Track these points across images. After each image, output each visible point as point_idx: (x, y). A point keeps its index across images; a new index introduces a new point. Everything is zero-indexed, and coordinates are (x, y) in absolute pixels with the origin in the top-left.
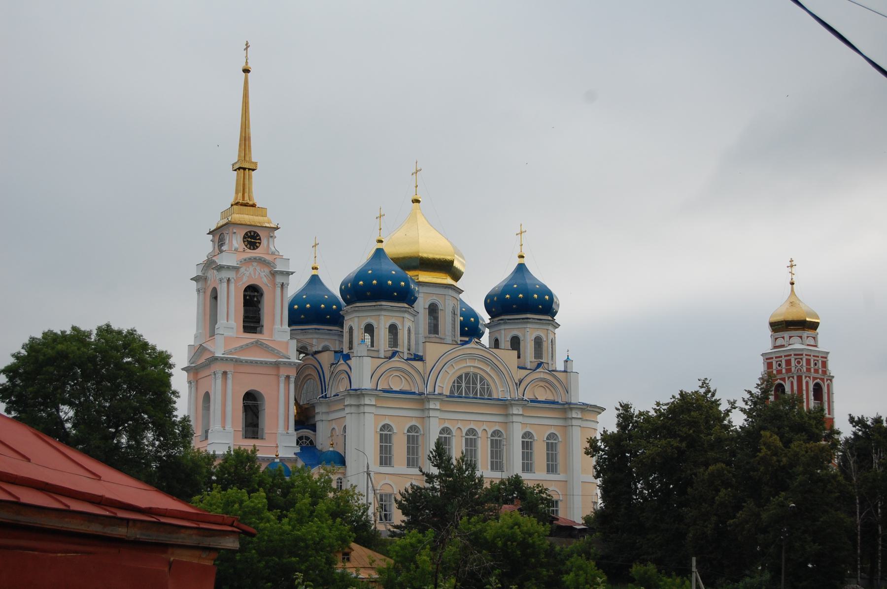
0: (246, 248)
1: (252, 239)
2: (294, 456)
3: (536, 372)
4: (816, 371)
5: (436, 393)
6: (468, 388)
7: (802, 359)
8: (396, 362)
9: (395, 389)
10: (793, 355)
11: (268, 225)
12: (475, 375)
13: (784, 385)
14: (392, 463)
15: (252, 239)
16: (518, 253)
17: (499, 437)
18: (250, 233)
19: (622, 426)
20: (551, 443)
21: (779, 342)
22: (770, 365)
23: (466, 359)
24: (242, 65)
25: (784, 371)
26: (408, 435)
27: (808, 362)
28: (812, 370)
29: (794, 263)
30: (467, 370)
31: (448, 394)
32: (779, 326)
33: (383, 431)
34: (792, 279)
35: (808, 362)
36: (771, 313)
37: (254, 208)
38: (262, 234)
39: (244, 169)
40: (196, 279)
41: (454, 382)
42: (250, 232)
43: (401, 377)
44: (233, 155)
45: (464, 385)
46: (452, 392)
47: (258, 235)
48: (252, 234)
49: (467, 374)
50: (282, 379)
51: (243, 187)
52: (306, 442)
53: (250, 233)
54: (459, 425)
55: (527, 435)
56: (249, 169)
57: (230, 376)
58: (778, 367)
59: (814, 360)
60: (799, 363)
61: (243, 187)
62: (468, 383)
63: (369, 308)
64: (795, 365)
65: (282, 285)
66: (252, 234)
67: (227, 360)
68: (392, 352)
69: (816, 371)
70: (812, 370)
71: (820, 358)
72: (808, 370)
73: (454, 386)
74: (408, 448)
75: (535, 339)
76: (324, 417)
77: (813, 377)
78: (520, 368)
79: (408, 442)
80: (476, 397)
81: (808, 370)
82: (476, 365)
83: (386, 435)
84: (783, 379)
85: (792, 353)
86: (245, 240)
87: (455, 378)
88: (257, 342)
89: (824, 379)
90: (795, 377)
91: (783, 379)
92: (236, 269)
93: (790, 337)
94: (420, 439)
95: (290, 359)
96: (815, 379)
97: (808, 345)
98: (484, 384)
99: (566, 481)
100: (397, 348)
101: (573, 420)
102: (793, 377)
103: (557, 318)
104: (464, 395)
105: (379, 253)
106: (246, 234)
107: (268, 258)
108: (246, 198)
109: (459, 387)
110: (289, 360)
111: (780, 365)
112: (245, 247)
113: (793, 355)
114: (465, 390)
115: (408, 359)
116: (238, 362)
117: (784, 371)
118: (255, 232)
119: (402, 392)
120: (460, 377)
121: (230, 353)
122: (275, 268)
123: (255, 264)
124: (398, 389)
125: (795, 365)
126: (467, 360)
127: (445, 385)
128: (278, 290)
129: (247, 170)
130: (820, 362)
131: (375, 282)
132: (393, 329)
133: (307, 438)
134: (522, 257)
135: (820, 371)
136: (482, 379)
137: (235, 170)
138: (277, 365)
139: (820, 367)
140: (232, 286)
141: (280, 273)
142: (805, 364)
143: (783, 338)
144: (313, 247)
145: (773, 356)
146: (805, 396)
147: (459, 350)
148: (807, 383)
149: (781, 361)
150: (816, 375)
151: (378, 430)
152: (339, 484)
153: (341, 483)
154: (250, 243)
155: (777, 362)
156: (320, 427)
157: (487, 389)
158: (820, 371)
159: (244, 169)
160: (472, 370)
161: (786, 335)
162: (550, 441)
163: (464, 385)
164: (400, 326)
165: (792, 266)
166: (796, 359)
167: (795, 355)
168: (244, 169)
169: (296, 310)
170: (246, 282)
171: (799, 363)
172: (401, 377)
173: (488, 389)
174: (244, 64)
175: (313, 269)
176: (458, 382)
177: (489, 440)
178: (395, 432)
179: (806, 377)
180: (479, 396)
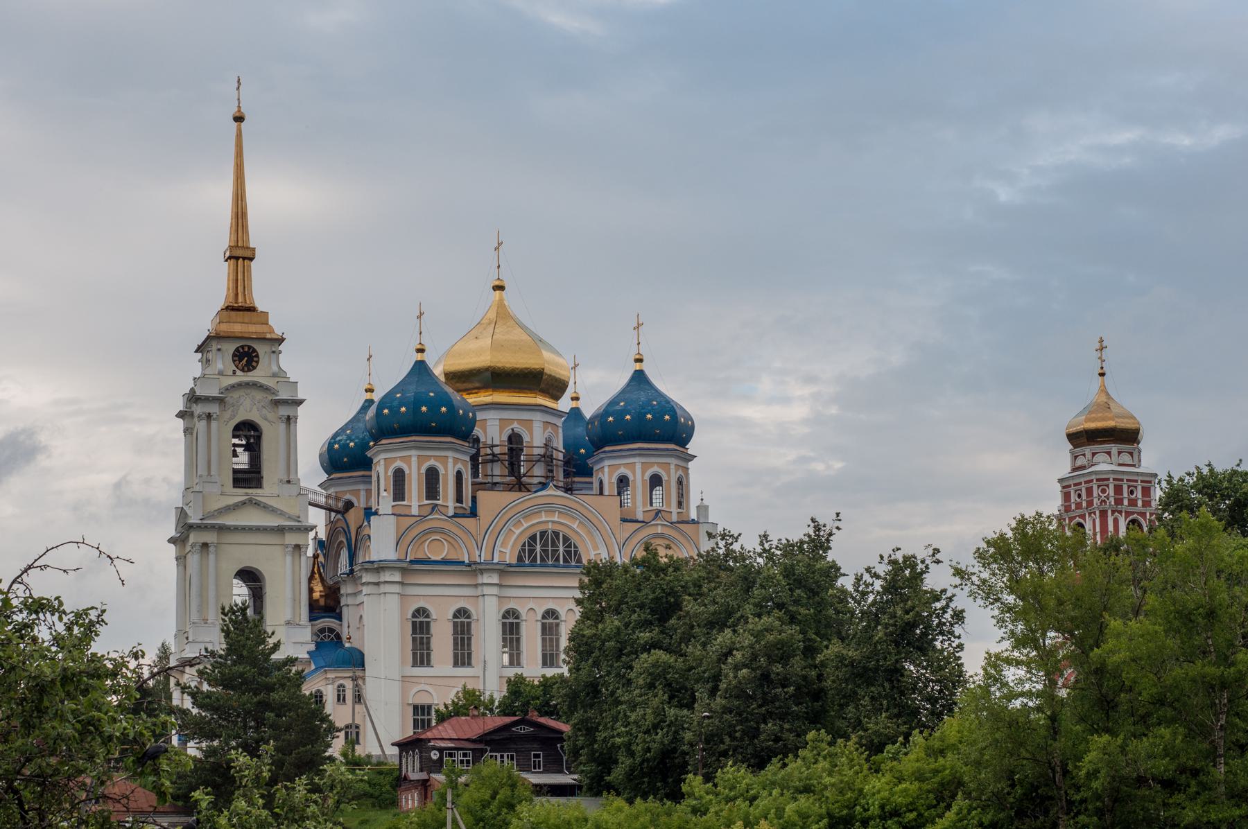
0: (237, 370)
1: (246, 358)
2: (307, 656)
4: (1133, 503)
5: (495, 561)
6: (545, 551)
7: (1108, 486)
8: (436, 520)
9: (433, 558)
10: (1095, 481)
11: (268, 336)
12: (556, 534)
13: (1084, 523)
14: (432, 664)
15: (246, 358)
16: (633, 356)
17: (426, 617)
18: (243, 349)
20: (420, 622)
21: (1080, 462)
22: (1067, 497)
24: (233, 110)
25: (1084, 504)
26: (413, 622)
27: (1118, 489)
28: (1126, 502)
29: (1104, 345)
30: (542, 527)
32: (1081, 439)
33: (508, 618)
34: (1102, 368)
35: (1118, 489)
37: (253, 313)
38: (261, 349)
39: (240, 256)
40: (181, 415)
41: (524, 545)
42: (243, 347)
44: (223, 240)
45: (538, 548)
46: (520, 559)
47: (254, 351)
48: (246, 349)
49: (543, 533)
51: (240, 282)
52: (329, 636)
53: (243, 349)
54: (531, 605)
55: (511, 613)
56: (244, 259)
58: (1077, 499)
59: (1129, 487)
60: (1104, 491)
61: (240, 282)
62: (545, 545)
64: (1099, 495)
65: (288, 418)
66: (246, 349)
67: (206, 527)
68: (431, 506)
69: (1133, 503)
70: (1126, 502)
71: (1125, 481)
72: (1119, 502)
73: (524, 551)
74: (455, 640)
76: (350, 601)
77: (1126, 512)
78: (624, 520)
79: (455, 632)
80: (557, 564)
81: (1119, 502)
82: (556, 519)
83: (421, 623)
84: (1083, 517)
85: (1093, 477)
87: (525, 538)
88: (250, 500)
89: (1145, 513)
90: (1098, 513)
91: (1083, 517)
92: (220, 401)
93: (1094, 454)
94: (473, 626)
95: (299, 521)
96: (1128, 514)
97: (1120, 465)
98: (569, 546)
100: (403, 500)
102: (1095, 513)
103: (692, 448)
104: (539, 562)
105: (421, 368)
106: (237, 350)
107: (270, 383)
108: (240, 299)
109: (531, 552)
110: (299, 524)
111: (1079, 496)
112: (235, 369)
113: (1095, 481)
114: (541, 554)
115: (456, 515)
116: (222, 529)
117: (1084, 504)
118: (250, 347)
119: (445, 562)
120: (533, 538)
121: (211, 515)
122: (277, 396)
124: (438, 558)
125: (1099, 495)
127: (508, 552)
129: (241, 260)
130: (1140, 488)
132: (432, 477)
133: (331, 630)
134: (639, 360)
135: (1140, 503)
136: (566, 539)
137: (226, 261)
138: (281, 530)
139: (1140, 496)
142: (1112, 493)
143: (1084, 455)
144: (634, 329)
145: (1071, 482)
147: (530, 499)
148: (1116, 521)
149: (1081, 490)
150: (1131, 509)
151: (409, 616)
153: (344, 691)
155: (1076, 491)
156: (346, 612)
157: (572, 553)
158: (1140, 503)
159: (237, 258)
160: (550, 526)
161: (1088, 451)
162: (418, 620)
163: (538, 548)
164: (442, 471)
165: (1102, 349)
166: (1099, 486)
167: (1098, 480)
168: (240, 256)
169: (337, 451)
171: (1104, 491)
173: (576, 552)
174: (236, 109)
175: (366, 391)
176: (530, 545)
177: (539, 625)
178: (434, 617)
179: (1113, 512)
180: (561, 563)
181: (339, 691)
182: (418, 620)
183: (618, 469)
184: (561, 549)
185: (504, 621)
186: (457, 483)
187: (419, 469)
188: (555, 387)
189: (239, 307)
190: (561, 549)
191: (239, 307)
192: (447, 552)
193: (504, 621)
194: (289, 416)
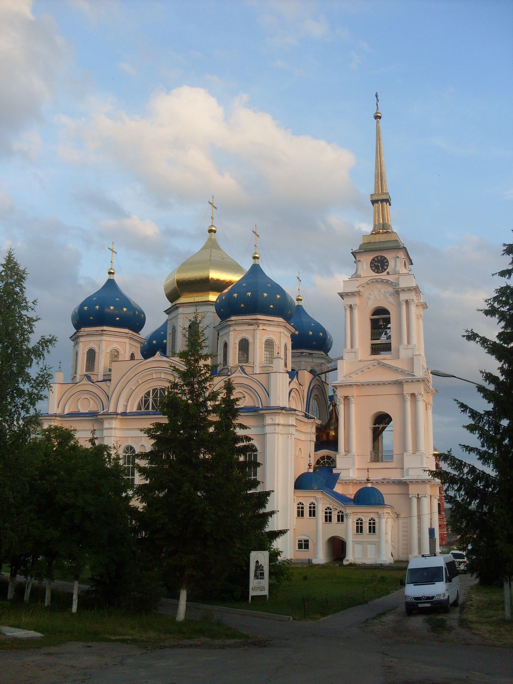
3: (80, 385)
9: (82, 411)
19: (152, 437)
23: (152, 374)
31: (135, 410)
36: (165, 295)
41: (142, 398)
42: (377, 257)
43: (89, 399)
46: (139, 408)
47: (385, 258)
50: (408, 398)
57: (420, 398)
63: (121, 334)
66: (379, 258)
75: (266, 341)
86: (372, 265)
87: (143, 394)
99: (431, 497)
101: (113, 431)
106: (373, 259)
118: (382, 257)
120: (148, 394)
123: (379, 286)
126: (154, 374)
128: (404, 307)
131: (97, 307)
138: (399, 383)
140: (356, 312)
141: (352, 295)
146: (278, 382)
152: (300, 510)
154: (377, 267)
163: (151, 400)
170: (372, 305)
172: (89, 399)
181: (298, 508)
187: (261, 340)
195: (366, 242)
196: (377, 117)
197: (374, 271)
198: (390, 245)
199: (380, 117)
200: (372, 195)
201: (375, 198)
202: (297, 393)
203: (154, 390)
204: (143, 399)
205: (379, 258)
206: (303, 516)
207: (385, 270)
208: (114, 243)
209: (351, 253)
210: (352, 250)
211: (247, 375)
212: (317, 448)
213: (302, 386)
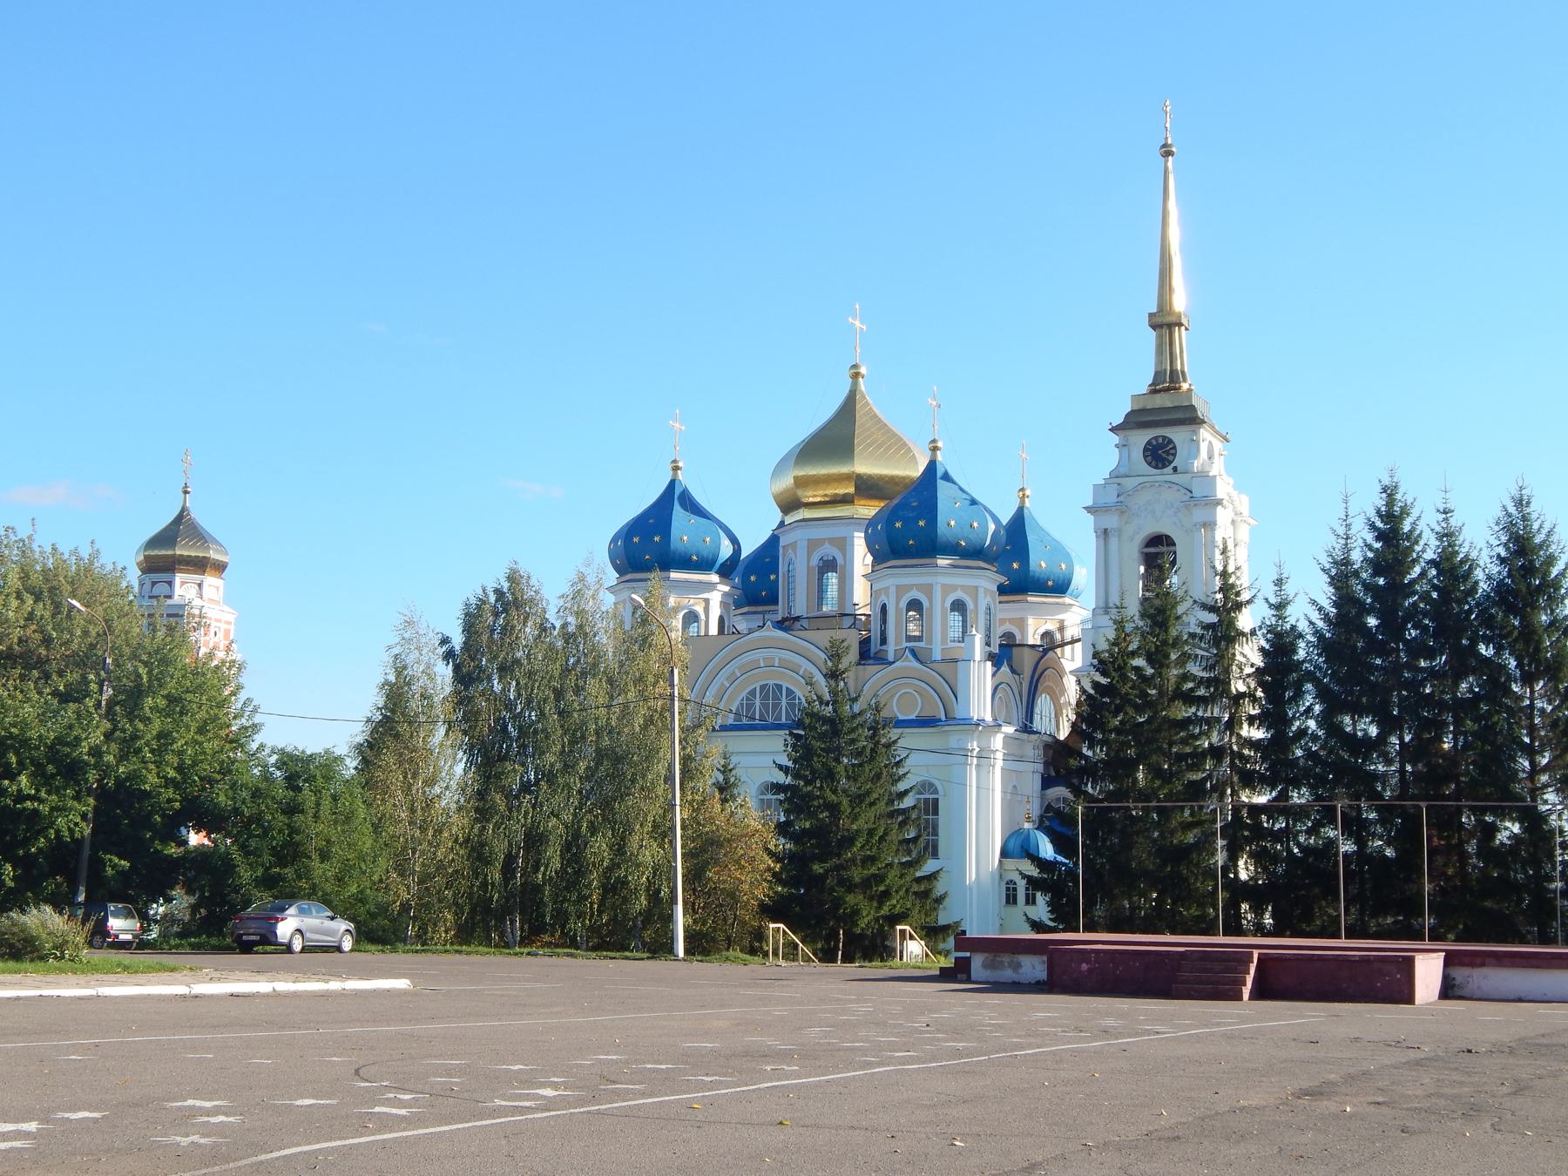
1: (1159, 455)
41: (743, 700)
42: (1156, 438)
47: (1170, 441)
61: (1166, 348)
62: (766, 697)
106: (1149, 443)
118: (1164, 438)
120: (753, 693)
163: (758, 702)
181: (1008, 889)
182: (922, 796)
183: (908, 591)
184: (784, 702)
185: (762, 797)
186: (932, 616)
188: (1191, 492)
189: (1167, 379)
190: (784, 702)
191: (1167, 379)
192: (922, 703)
193: (762, 797)
194: (1106, 530)
195: (1136, 408)
196: (186, 492)
197: (1149, 464)
198: (1179, 415)
199: (188, 493)
200: (1151, 315)
201: (1159, 320)
202: (1008, 689)
203: (763, 687)
204: (745, 702)
205: (1160, 440)
206: (1016, 904)
207: (1170, 462)
208: (36, 522)
209: (1110, 430)
210: (1111, 424)
211: (921, 663)
212: (1047, 783)
213: (1019, 675)
